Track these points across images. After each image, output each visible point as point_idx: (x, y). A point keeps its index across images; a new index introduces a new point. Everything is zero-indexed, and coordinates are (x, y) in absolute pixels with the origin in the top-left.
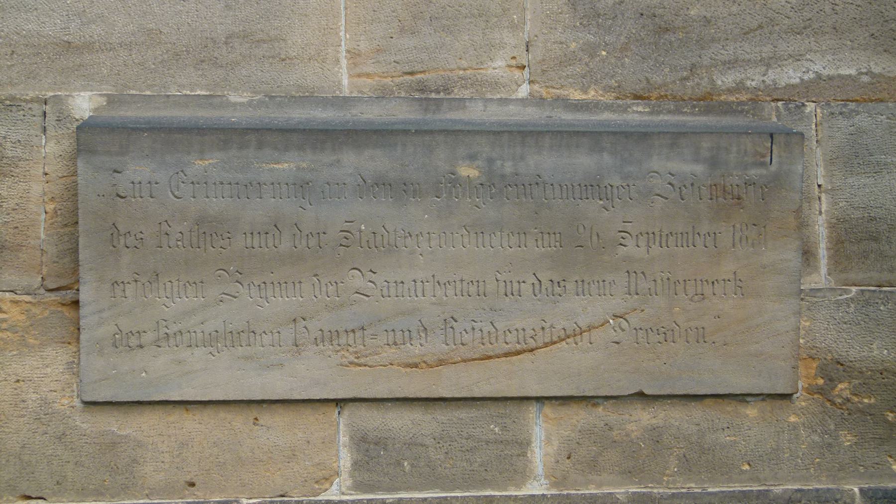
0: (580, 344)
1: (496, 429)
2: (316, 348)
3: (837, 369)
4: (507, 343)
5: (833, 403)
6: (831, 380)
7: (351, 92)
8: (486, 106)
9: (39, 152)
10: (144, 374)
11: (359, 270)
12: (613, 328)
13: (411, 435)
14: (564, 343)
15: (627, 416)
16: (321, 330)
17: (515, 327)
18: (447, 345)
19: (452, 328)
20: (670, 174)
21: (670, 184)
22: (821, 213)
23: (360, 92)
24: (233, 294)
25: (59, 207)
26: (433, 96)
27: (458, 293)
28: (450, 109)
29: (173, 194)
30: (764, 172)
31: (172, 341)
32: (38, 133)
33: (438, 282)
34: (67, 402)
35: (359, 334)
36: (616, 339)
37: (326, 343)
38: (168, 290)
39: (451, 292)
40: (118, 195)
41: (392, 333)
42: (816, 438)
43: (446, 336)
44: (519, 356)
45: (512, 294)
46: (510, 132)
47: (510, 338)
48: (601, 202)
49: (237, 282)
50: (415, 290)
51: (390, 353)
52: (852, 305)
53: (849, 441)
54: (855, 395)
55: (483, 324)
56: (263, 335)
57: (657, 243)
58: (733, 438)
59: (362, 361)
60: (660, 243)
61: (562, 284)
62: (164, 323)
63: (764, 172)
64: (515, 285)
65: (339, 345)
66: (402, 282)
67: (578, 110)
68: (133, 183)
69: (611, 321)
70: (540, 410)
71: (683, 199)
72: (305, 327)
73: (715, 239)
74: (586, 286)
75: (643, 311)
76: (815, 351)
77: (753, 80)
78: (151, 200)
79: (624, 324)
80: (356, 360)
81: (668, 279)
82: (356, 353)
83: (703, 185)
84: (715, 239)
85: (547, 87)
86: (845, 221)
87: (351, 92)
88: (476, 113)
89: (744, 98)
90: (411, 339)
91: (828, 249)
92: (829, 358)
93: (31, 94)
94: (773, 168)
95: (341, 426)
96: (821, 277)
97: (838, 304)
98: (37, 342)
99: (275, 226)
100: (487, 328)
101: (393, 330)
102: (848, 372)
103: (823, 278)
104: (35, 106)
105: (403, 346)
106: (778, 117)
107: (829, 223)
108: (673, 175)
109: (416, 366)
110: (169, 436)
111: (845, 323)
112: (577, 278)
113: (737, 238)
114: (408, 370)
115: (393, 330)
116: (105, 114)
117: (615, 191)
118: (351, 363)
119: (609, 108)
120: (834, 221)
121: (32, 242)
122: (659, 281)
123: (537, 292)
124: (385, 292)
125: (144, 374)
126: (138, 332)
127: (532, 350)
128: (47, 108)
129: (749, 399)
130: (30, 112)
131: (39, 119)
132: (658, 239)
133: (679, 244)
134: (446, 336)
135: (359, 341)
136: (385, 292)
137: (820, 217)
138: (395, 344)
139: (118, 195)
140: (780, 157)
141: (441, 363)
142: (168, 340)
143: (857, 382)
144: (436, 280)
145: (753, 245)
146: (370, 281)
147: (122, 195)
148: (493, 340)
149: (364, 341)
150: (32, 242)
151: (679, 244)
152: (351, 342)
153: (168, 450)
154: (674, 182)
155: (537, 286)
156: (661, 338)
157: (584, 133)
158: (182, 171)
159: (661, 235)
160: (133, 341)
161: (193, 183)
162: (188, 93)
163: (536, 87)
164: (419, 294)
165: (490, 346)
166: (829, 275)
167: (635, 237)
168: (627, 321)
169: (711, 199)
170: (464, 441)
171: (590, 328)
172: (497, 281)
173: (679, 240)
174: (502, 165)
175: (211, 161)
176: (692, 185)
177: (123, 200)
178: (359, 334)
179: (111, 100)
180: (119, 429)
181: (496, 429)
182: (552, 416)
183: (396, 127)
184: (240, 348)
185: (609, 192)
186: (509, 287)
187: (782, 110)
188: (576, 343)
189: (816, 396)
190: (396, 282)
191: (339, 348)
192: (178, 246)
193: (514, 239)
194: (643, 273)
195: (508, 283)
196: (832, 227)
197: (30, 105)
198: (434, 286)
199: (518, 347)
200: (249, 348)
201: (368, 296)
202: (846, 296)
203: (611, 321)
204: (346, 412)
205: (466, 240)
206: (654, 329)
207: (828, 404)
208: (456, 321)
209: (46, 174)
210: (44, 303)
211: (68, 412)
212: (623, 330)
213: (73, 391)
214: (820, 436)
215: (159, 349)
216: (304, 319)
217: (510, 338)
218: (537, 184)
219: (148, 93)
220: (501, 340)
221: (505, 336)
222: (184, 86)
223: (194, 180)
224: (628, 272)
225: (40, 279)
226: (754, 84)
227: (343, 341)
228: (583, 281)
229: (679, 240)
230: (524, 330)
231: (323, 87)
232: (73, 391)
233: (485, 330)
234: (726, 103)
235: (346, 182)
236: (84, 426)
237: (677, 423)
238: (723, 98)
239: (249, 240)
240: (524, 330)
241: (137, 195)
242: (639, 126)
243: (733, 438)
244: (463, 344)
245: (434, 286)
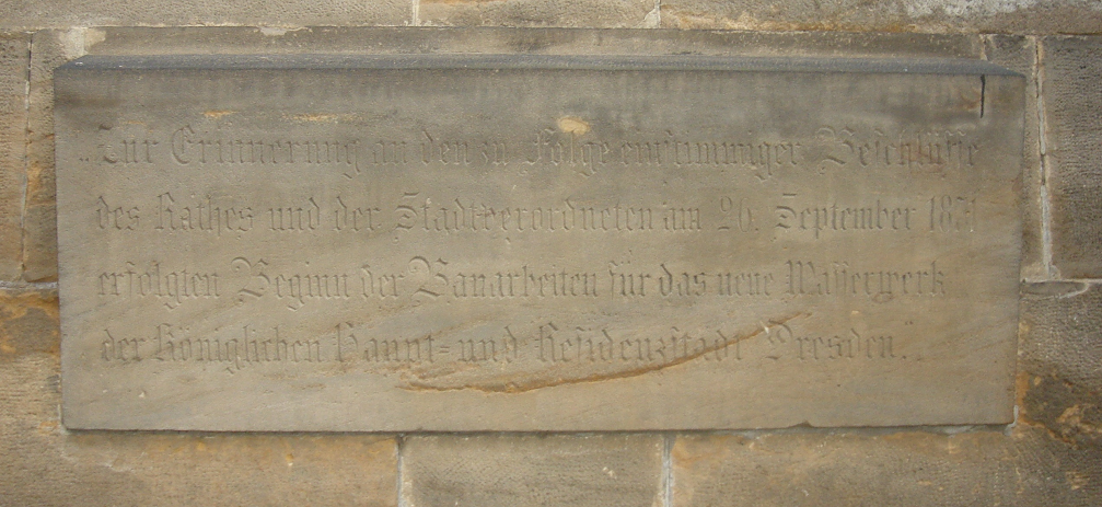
0: (724, 359)
1: (611, 473)
2: (367, 363)
3: (1066, 390)
4: (624, 359)
5: (1059, 434)
6: (1056, 404)
7: (424, 22)
8: (601, 39)
9: (22, 103)
10: (142, 395)
11: (424, 260)
12: (769, 338)
13: (496, 480)
14: (702, 358)
15: (787, 456)
16: (373, 340)
17: (636, 337)
18: (544, 360)
19: (550, 337)
20: (848, 129)
21: (847, 143)
22: (1044, 181)
23: (434, 21)
24: (256, 290)
25: (44, 174)
26: (532, 25)
27: (559, 291)
28: (553, 43)
29: (177, 157)
30: (973, 127)
31: (177, 351)
32: (21, 79)
33: (531, 276)
34: (48, 428)
35: (424, 345)
36: (773, 353)
37: (380, 357)
38: (172, 285)
39: (548, 289)
40: (106, 159)
41: (469, 344)
42: (1036, 482)
43: (542, 349)
44: (641, 376)
45: (632, 292)
46: (630, 71)
47: (629, 351)
48: (754, 168)
49: (261, 274)
50: (500, 287)
51: (468, 372)
52: (1085, 305)
53: (1077, 484)
54: (1087, 423)
55: (593, 333)
56: (297, 345)
57: (830, 224)
58: (927, 483)
59: (429, 381)
60: (834, 222)
61: (700, 278)
62: (167, 329)
63: (973, 127)
64: (637, 280)
65: (398, 360)
66: (482, 276)
67: (725, 44)
68: (125, 142)
69: (767, 329)
70: (669, 448)
71: (865, 164)
72: (352, 336)
73: (907, 218)
74: (733, 282)
75: (809, 315)
76: (1036, 366)
77: (954, 6)
78: (149, 165)
79: (784, 333)
80: (420, 381)
81: (844, 272)
82: (420, 371)
83: (892, 145)
84: (907, 218)
85: (684, 13)
86: (1075, 193)
87: (424, 22)
88: (587, 49)
89: (941, 30)
90: (494, 352)
91: (1054, 230)
92: (1053, 374)
93: (16, 29)
94: (985, 122)
95: (403, 467)
96: (1044, 268)
97: (1067, 303)
98: (13, 350)
99: (311, 199)
100: (598, 338)
101: (470, 341)
102: (1078, 393)
103: (1047, 268)
104: (18, 44)
105: (484, 362)
106: (989, 54)
107: (1054, 194)
108: (851, 131)
109: (500, 388)
110: (178, 476)
111: (1076, 328)
112: (720, 270)
113: (936, 215)
114: (492, 394)
115: (470, 341)
116: (104, 52)
117: (773, 152)
118: (414, 384)
119: (765, 40)
120: (1061, 192)
121: (11, 220)
122: (831, 275)
123: (666, 289)
124: (459, 288)
125: (142, 395)
126: (134, 340)
127: (660, 368)
128: (33, 47)
129: (948, 430)
130: (12, 52)
131: (21, 61)
132: (830, 218)
133: (859, 225)
134: (542, 349)
135: (424, 355)
136: (459, 288)
137: (1042, 188)
138: (473, 358)
139: (106, 159)
140: (994, 106)
141: (536, 384)
142: (173, 351)
143: (1090, 406)
144: (528, 273)
145: (958, 226)
146: (440, 275)
147: (112, 158)
148: (606, 355)
149: (431, 355)
150: (11, 220)
151: (859, 225)
152: (413, 356)
153: (176, 493)
154: (853, 141)
155: (666, 282)
156: (834, 351)
157: (730, 73)
158: (188, 126)
159: (834, 214)
160: (128, 352)
161: (202, 142)
162: (212, 24)
163: (669, 14)
164: (506, 292)
165: (602, 362)
166: (1054, 264)
167: (799, 215)
168: (789, 329)
169: (902, 163)
170: (566, 488)
171: (739, 338)
172: (612, 274)
173: (859, 219)
174: (618, 117)
175: (226, 113)
176: (877, 144)
177: (112, 166)
178: (424, 345)
179: (114, 36)
180: (114, 464)
181: (611, 473)
182: (685, 454)
183: (476, 65)
184: (266, 362)
185: (764, 155)
186: (627, 284)
187: (993, 45)
188: (719, 359)
189: (1037, 426)
190: (474, 276)
191: (398, 364)
192: (183, 226)
193: (634, 218)
194: (810, 263)
195: (627, 278)
196: (1058, 200)
197: (11, 44)
198: (526, 282)
199: (641, 364)
200: (278, 363)
201: (437, 295)
202: (1077, 293)
203: (767, 329)
204: (409, 449)
205: (569, 219)
206: (825, 339)
207: (1052, 435)
208: (556, 329)
209: (30, 132)
210: (20, 299)
211: (51, 442)
212: (783, 341)
213: (56, 414)
214: (1041, 479)
215: (162, 363)
216: (351, 325)
217: (629, 351)
218: (666, 142)
219: (162, 25)
220: (616, 354)
221: (623, 349)
222: (207, 16)
223: (204, 138)
224: (789, 262)
225: (20, 268)
226: (956, 11)
227: (403, 354)
228: (728, 275)
229: (859, 219)
230: (648, 340)
231: (387, 14)
232: (56, 414)
233: (595, 341)
234: (925, 37)
235: (406, 140)
236: (72, 460)
237: (853, 465)
238: (917, 28)
239: (276, 217)
240: (648, 340)
241: (130, 159)
242: (806, 64)
243: (927, 483)
244: (565, 360)
245: (526, 282)
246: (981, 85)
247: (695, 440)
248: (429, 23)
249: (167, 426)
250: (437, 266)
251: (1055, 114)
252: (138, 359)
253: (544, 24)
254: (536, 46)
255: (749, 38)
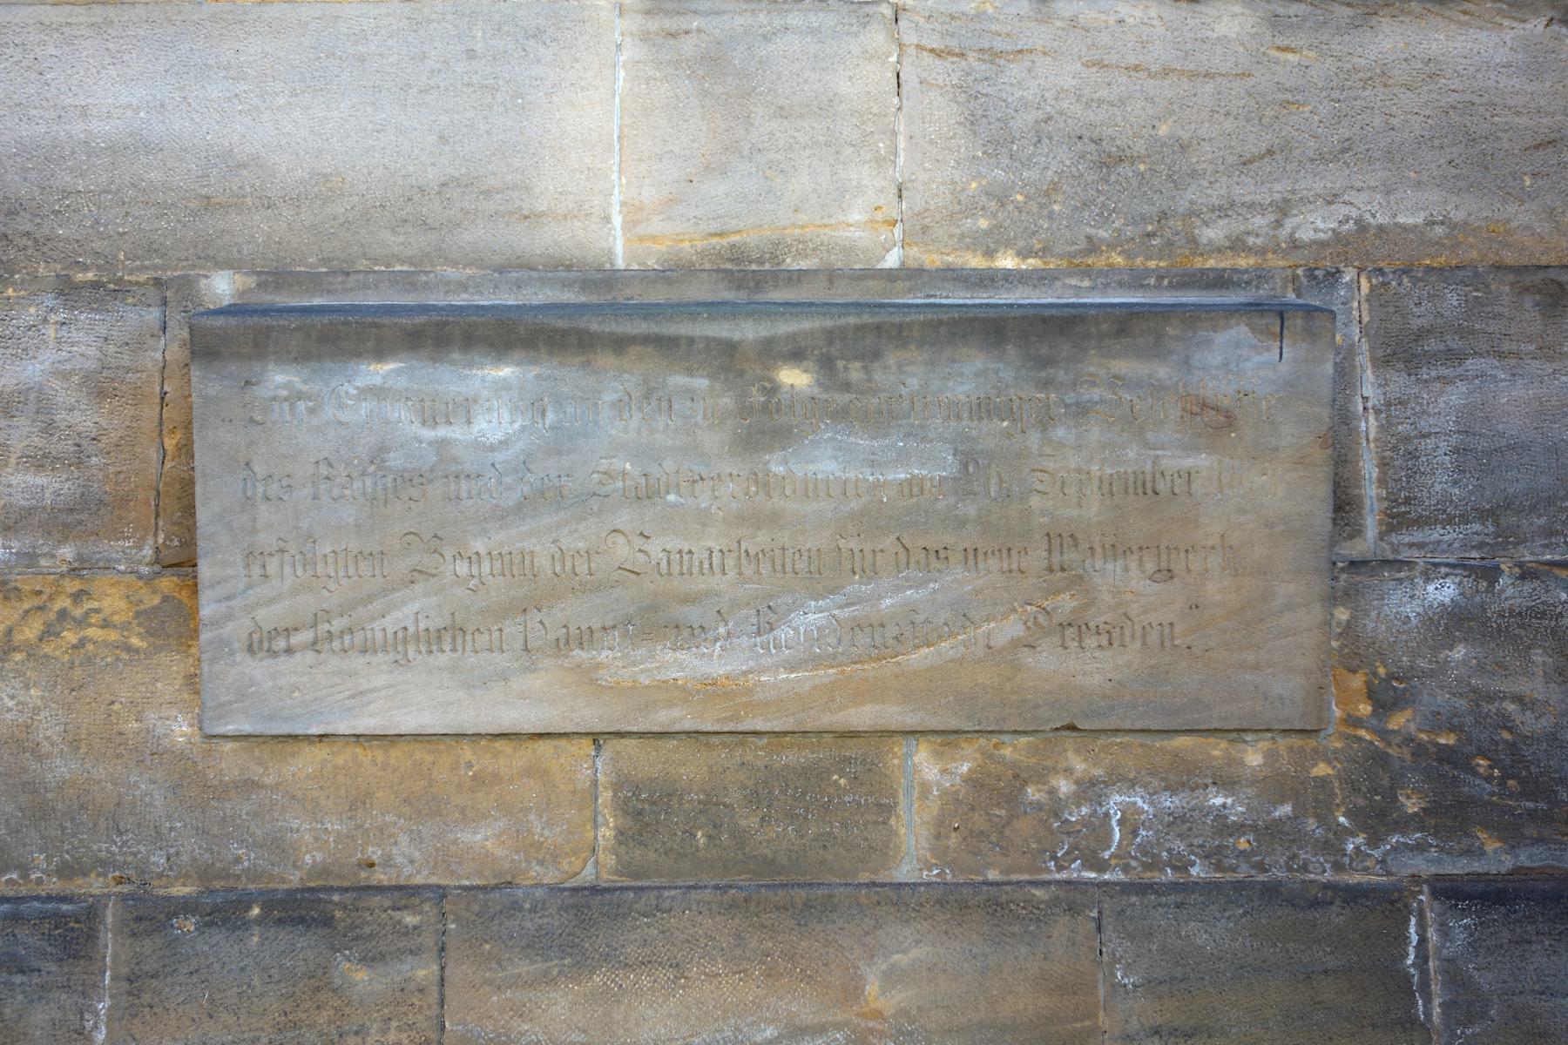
1: (842, 781)
26: (754, 267)
61: (942, 554)
64: (869, 556)
72: (541, 622)
160: (280, 644)
163: (914, 251)
177: (259, 428)
181: (842, 781)
246: (1278, 323)
247: (942, 745)
248: (635, 267)
249: (316, 730)
250: (639, 542)
251: (1374, 360)
252: (289, 651)
253: (767, 266)
254: (1355, 727)
255: (1008, 277)
